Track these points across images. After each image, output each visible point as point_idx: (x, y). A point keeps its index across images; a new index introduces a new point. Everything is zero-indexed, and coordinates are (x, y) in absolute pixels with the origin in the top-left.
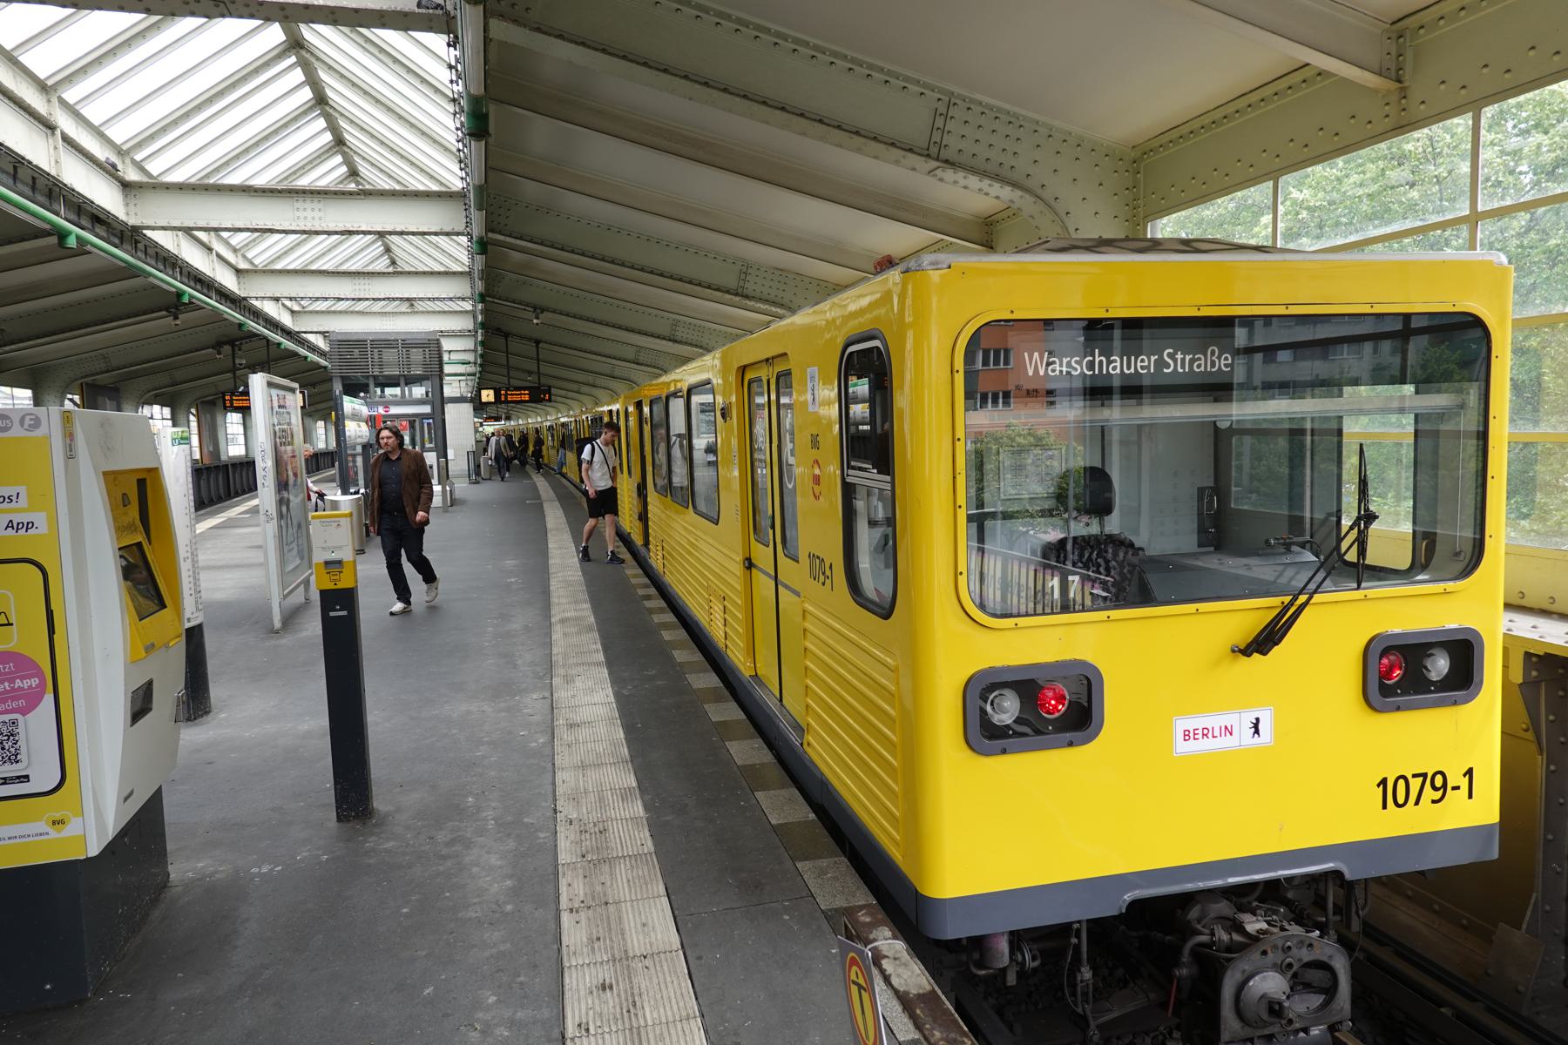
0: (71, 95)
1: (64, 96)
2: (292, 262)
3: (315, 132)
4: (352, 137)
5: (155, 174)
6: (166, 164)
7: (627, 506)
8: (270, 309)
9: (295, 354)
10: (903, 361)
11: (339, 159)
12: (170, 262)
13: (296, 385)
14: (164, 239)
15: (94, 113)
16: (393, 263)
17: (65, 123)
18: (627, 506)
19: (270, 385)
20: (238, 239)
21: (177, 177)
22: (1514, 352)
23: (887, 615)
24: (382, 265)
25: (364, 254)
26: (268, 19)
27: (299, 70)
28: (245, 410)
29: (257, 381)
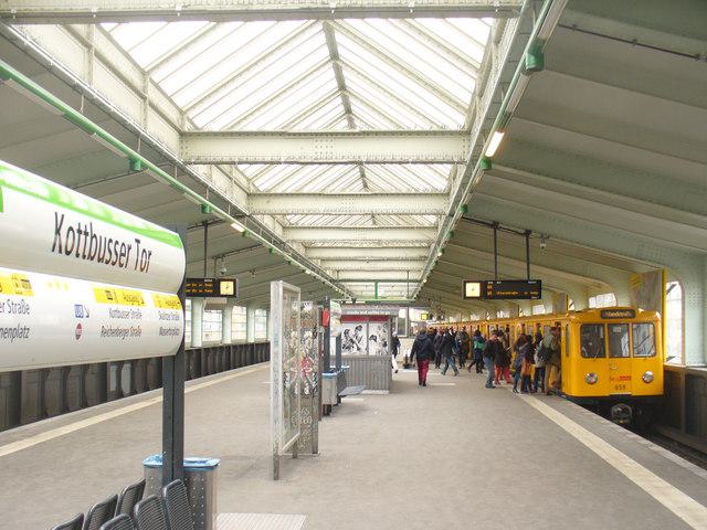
0: (156, 77)
1: (153, 78)
2: (334, 224)
3: (337, 107)
4: (351, 80)
5: (200, 126)
6: (204, 120)
7: (324, 150)
8: (267, 222)
9: (260, 244)
10: (591, 429)
11: (340, 100)
12: (202, 187)
13: (298, 289)
14: (200, 171)
15: (168, 87)
16: (365, 186)
17: (152, 94)
18: (324, 150)
19: (285, 290)
20: (251, 170)
21: (216, 128)
22: (106, 401)
23: (487, 386)
24: (357, 188)
25: (347, 179)
26: (318, 19)
27: (323, 35)
28: (267, 307)
29: (277, 288)
